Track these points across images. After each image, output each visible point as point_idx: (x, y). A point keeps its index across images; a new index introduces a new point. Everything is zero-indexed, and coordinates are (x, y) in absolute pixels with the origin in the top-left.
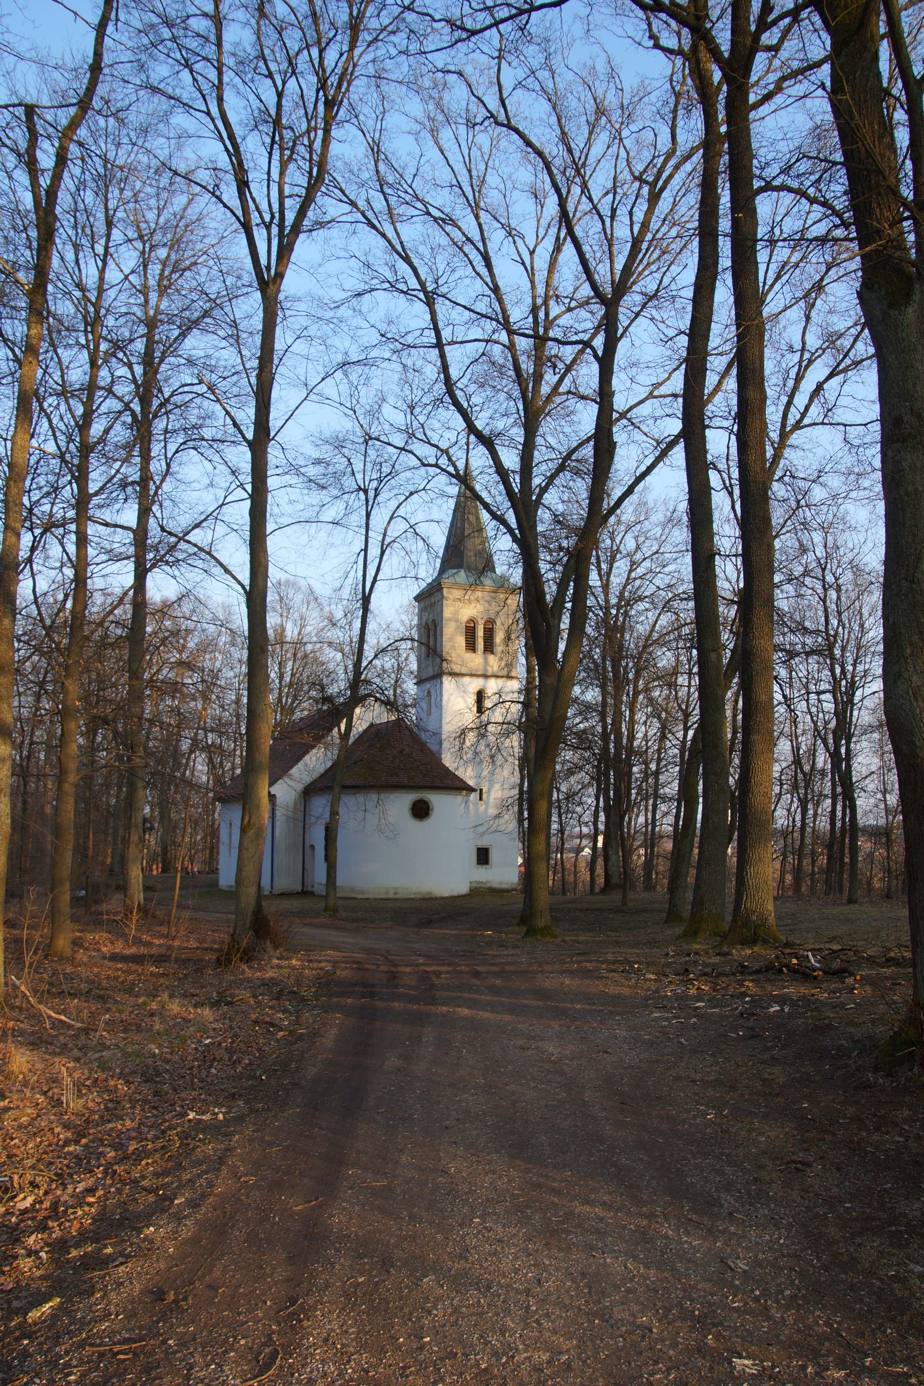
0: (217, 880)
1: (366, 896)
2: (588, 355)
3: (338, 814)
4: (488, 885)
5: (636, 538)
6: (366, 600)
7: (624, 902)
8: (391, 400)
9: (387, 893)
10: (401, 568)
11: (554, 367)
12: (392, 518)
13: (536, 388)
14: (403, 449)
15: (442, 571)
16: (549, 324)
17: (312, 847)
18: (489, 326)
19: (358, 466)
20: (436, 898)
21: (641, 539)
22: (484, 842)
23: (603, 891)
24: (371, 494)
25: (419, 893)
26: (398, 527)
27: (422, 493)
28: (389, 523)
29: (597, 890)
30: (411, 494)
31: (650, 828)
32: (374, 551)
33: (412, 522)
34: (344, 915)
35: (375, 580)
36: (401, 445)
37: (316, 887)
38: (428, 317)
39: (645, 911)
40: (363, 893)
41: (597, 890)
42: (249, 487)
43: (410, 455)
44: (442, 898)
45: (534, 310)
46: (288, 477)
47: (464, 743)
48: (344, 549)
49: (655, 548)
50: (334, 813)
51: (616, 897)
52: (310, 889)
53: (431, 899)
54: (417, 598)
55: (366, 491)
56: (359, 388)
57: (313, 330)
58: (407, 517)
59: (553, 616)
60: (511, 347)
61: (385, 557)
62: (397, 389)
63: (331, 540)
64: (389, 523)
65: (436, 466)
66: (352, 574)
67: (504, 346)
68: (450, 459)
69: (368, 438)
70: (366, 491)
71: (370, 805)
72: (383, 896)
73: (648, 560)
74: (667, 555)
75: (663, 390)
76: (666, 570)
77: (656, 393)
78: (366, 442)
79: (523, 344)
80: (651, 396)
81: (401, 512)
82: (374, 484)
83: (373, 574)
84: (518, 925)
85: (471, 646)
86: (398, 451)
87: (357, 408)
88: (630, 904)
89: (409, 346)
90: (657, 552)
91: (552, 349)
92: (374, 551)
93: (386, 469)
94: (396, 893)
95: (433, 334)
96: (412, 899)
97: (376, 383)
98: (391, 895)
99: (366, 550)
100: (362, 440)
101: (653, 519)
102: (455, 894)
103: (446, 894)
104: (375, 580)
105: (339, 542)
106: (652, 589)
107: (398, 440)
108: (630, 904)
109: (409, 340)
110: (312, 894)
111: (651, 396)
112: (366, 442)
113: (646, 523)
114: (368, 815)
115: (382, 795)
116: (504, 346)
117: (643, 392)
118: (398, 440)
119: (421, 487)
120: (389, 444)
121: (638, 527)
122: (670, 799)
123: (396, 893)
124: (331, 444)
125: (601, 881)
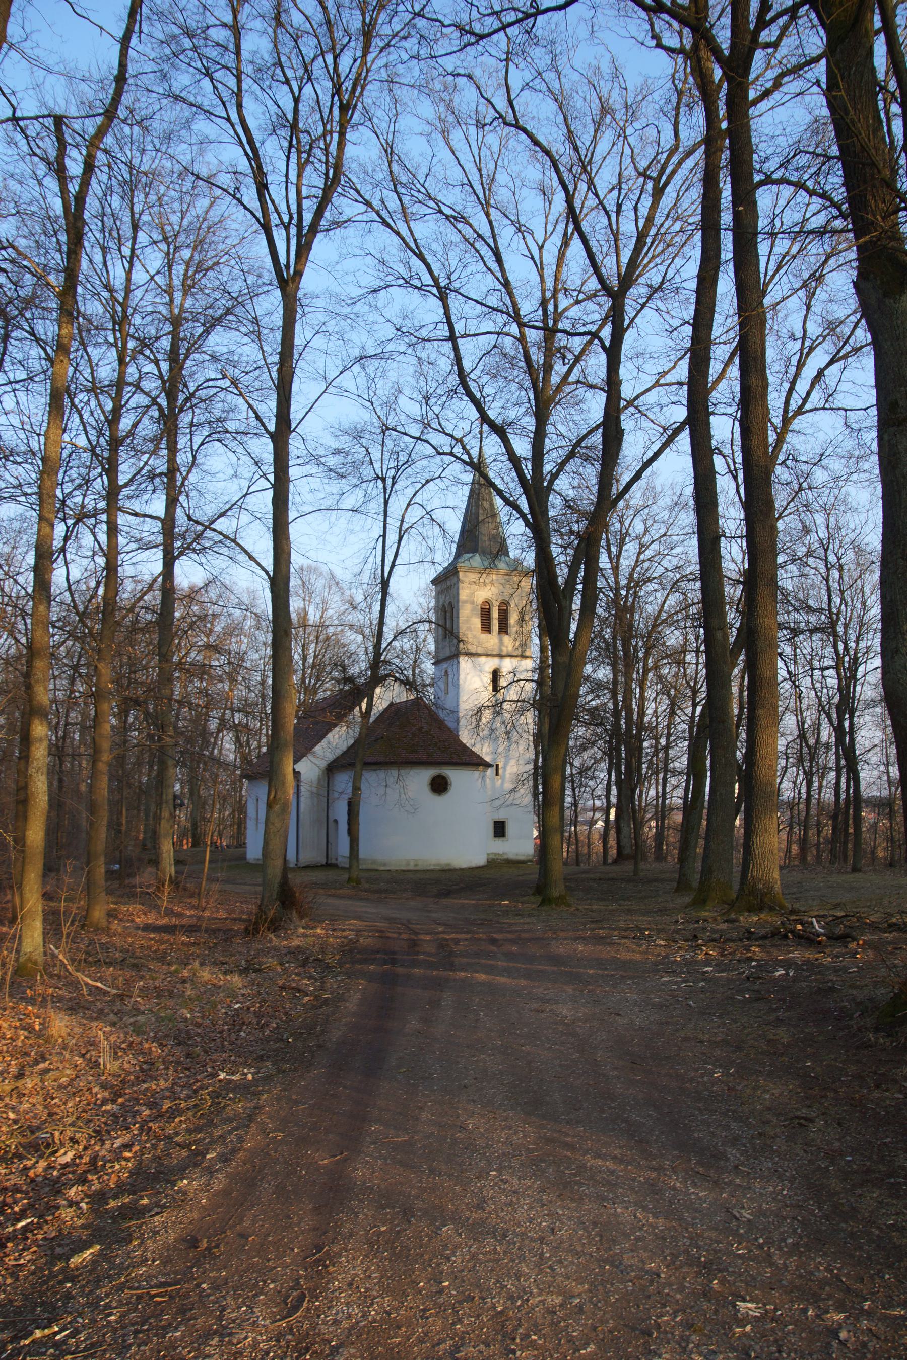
0: (245, 853)
3: (359, 789)
5: (645, 521)
6: (385, 584)
7: (636, 872)
8: (407, 391)
9: (408, 865)
10: (418, 553)
11: (564, 357)
12: (409, 505)
14: (418, 439)
15: (458, 555)
16: (558, 316)
17: (336, 821)
18: (501, 319)
19: (376, 455)
20: (455, 870)
21: (649, 523)
22: (501, 816)
23: (615, 862)
24: (389, 482)
29: (610, 861)
30: (427, 481)
32: (392, 537)
34: (367, 886)
35: (393, 565)
36: (417, 435)
37: (340, 859)
39: (656, 880)
40: (385, 865)
41: (610, 861)
42: (271, 477)
43: (426, 444)
44: (461, 870)
45: (544, 303)
46: (308, 467)
47: (480, 720)
48: (364, 535)
49: (663, 531)
50: (356, 789)
51: (628, 867)
52: (333, 861)
53: (450, 870)
54: (435, 582)
55: (384, 480)
57: (331, 326)
58: (424, 503)
59: (565, 597)
60: (522, 339)
61: (403, 543)
62: (413, 381)
63: (351, 527)
66: (371, 559)
68: (464, 448)
69: (385, 429)
70: (384, 480)
71: (391, 780)
74: (675, 538)
76: (674, 552)
77: (662, 382)
78: (383, 432)
79: (533, 336)
80: (657, 384)
81: (417, 499)
82: (392, 473)
84: (534, 894)
85: (486, 627)
86: (414, 440)
90: (665, 535)
91: (561, 340)
92: (392, 537)
93: (403, 458)
95: (447, 328)
96: (432, 871)
97: (392, 375)
98: (412, 867)
99: (384, 536)
100: (379, 431)
102: (473, 865)
103: (464, 865)
104: (393, 565)
105: (357, 529)
106: (660, 570)
107: (415, 430)
108: (642, 874)
111: (657, 384)
112: (383, 432)
113: (654, 506)
114: (389, 791)
115: (402, 771)
117: (649, 381)
118: (415, 430)
119: (437, 475)
120: (405, 434)
121: (646, 510)
125: (613, 852)
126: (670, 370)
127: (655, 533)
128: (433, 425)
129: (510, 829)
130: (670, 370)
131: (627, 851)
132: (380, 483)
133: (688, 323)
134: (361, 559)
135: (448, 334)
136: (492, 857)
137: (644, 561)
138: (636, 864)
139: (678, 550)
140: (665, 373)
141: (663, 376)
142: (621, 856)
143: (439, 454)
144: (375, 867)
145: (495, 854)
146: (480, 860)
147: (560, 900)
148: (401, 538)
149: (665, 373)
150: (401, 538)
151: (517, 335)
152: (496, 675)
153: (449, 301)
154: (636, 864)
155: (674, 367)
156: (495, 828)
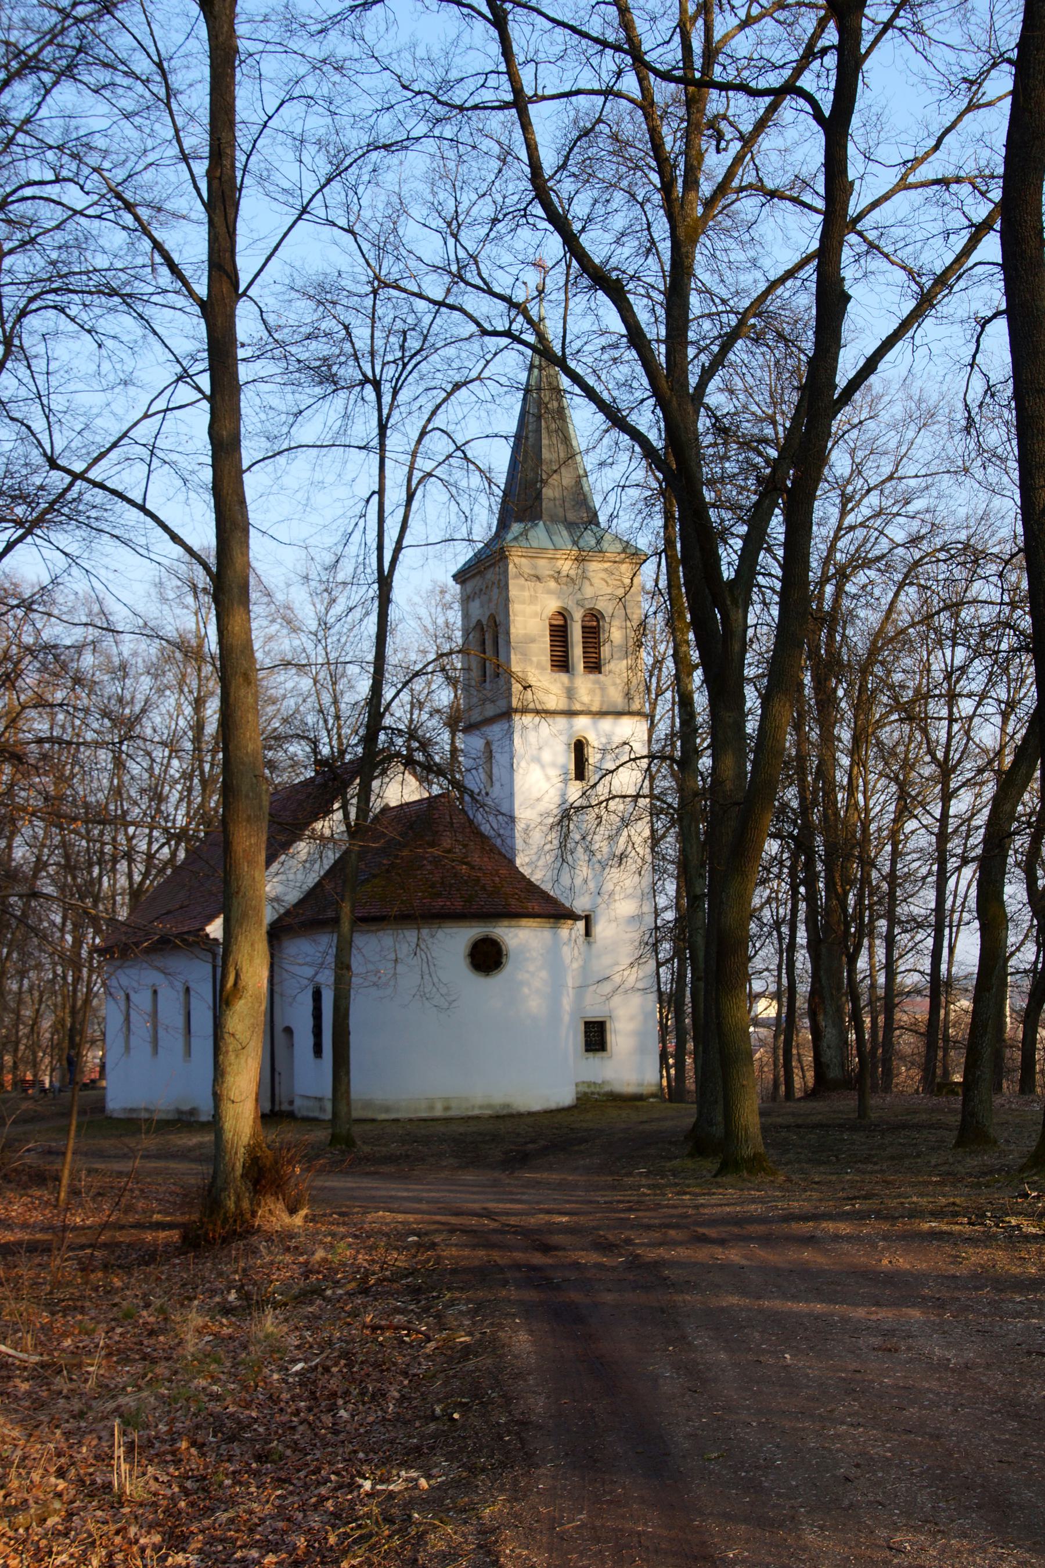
0: (102, 1100)
1: (393, 1116)
2: (791, 110)
3: (348, 968)
4: (607, 1089)
5: (852, 452)
6: (384, 583)
7: (862, 1109)
8: (418, 211)
9: (432, 1108)
10: (443, 523)
11: (720, 136)
12: (423, 434)
13: (691, 183)
14: (441, 304)
15: (503, 525)
16: (711, 53)
17: (288, 1031)
18: (609, 61)
19: (361, 334)
20: (520, 1115)
21: (860, 454)
22: (594, 1013)
23: (811, 1095)
24: (386, 388)
25: (489, 1106)
26: (438, 445)
27: (475, 386)
28: (419, 441)
29: (798, 1094)
30: (457, 386)
31: (881, 979)
32: (395, 495)
33: (460, 440)
34: (367, 1149)
35: (398, 548)
36: (439, 296)
37: (298, 1102)
38: (495, 49)
39: (904, 1126)
40: (387, 1109)
41: (798, 1094)
42: (204, 381)
43: (456, 314)
44: (530, 1114)
45: (683, 29)
46: (259, 363)
47: (567, 835)
48: (343, 492)
49: (887, 470)
50: (343, 967)
51: (845, 1103)
52: (285, 1107)
53: (511, 1116)
54: (460, 577)
55: (377, 385)
56: (361, 190)
57: (309, 86)
58: (450, 429)
59: (735, 602)
60: (646, 104)
61: (415, 505)
62: (424, 189)
63: (318, 476)
64: (419, 441)
65: (507, 334)
66: (356, 537)
67: (632, 101)
68: (529, 321)
69: (379, 284)
70: (377, 385)
71: (404, 950)
72: (424, 1115)
73: (875, 493)
74: (913, 483)
75: (926, 172)
76: (911, 508)
77: (911, 179)
78: (375, 292)
79: (664, 92)
80: (904, 185)
81: (438, 421)
82: (390, 372)
83: (395, 535)
84: (691, 1155)
85: (561, 663)
86: (433, 308)
87: (357, 229)
88: (873, 1116)
89: (461, 108)
90: (891, 478)
91: (715, 102)
92: (395, 495)
93: (413, 344)
94: (447, 1108)
95: (507, 86)
96: (477, 1118)
97: (389, 179)
98: (438, 1113)
99: (381, 492)
100: (368, 289)
101: (885, 416)
102: (552, 1105)
103: (536, 1106)
104: (398, 548)
105: (330, 478)
106: (884, 545)
107: (435, 287)
108: (873, 1116)
109: (459, 96)
110: (291, 1116)
111: (904, 185)
112: (375, 292)
113: (871, 424)
114: (400, 968)
115: (425, 932)
116: (632, 101)
117: (890, 178)
118: (435, 287)
119: (474, 374)
120: (420, 296)
121: (854, 433)
122: (920, 926)
123: (447, 1108)
124: (310, 297)
125: (804, 1078)
126: (927, 155)
127: (877, 470)
128: (468, 276)
129: (578, 1038)
130: (927, 155)
131: (834, 1073)
132: (369, 391)
133: (1009, 61)
134: (337, 537)
135: (509, 97)
136: (584, 1089)
137: (852, 528)
138: (862, 1098)
139: (917, 505)
140: (918, 161)
141: (913, 169)
142: (823, 1084)
143: (485, 332)
144: (370, 1115)
145: (589, 1084)
146: (566, 1097)
147: (755, 1165)
148: (410, 497)
149: (918, 161)
150: (410, 497)
151: (636, 93)
152: (579, 748)
153: (511, 25)
154: (862, 1098)
155: (936, 147)
156: (587, 1033)
